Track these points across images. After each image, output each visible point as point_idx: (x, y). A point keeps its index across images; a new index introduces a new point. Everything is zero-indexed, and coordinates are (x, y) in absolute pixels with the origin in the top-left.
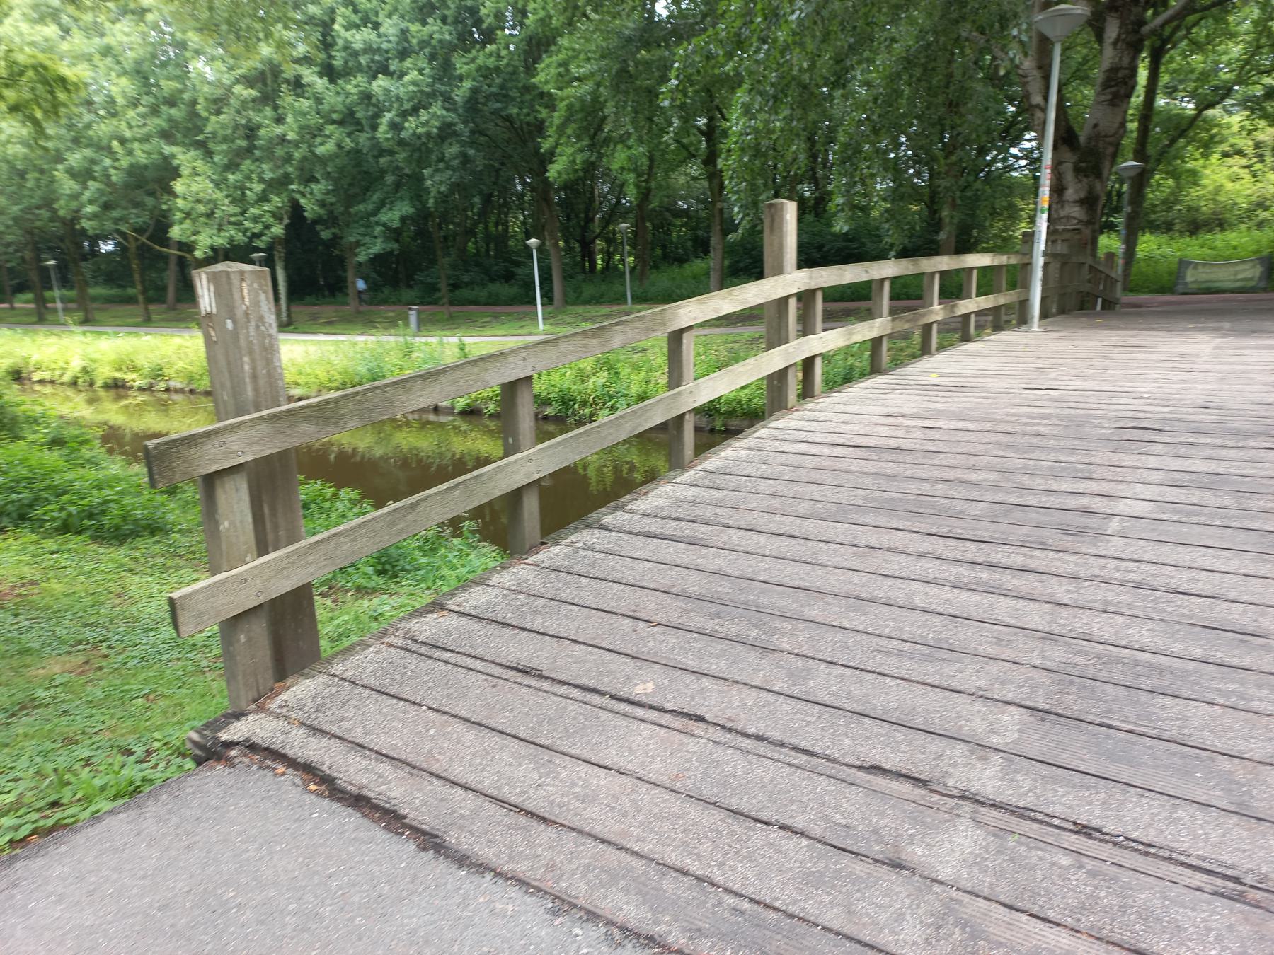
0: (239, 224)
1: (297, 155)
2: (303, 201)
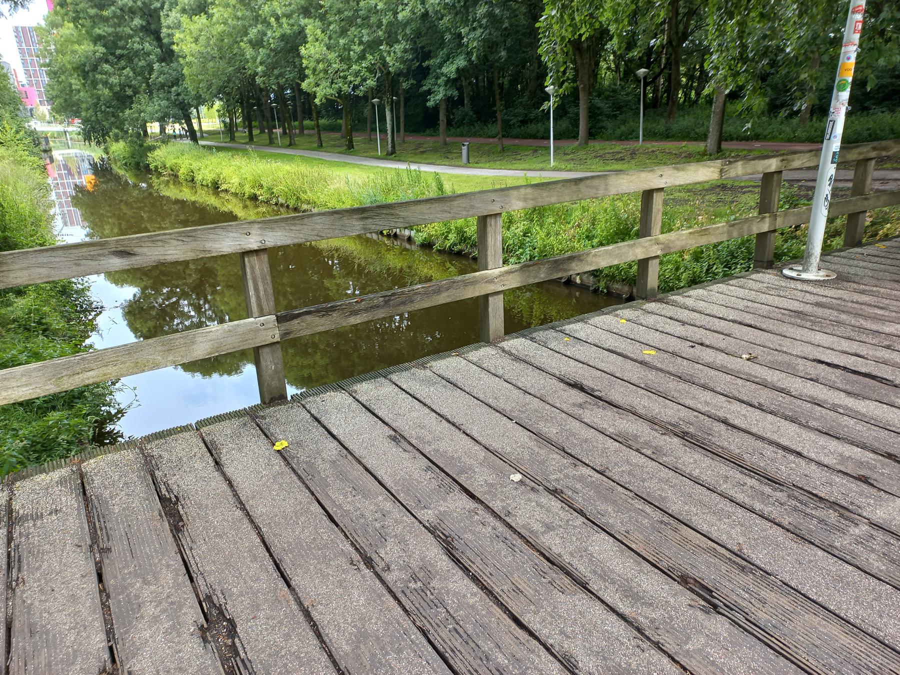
0: (345, 78)
2: (388, 59)
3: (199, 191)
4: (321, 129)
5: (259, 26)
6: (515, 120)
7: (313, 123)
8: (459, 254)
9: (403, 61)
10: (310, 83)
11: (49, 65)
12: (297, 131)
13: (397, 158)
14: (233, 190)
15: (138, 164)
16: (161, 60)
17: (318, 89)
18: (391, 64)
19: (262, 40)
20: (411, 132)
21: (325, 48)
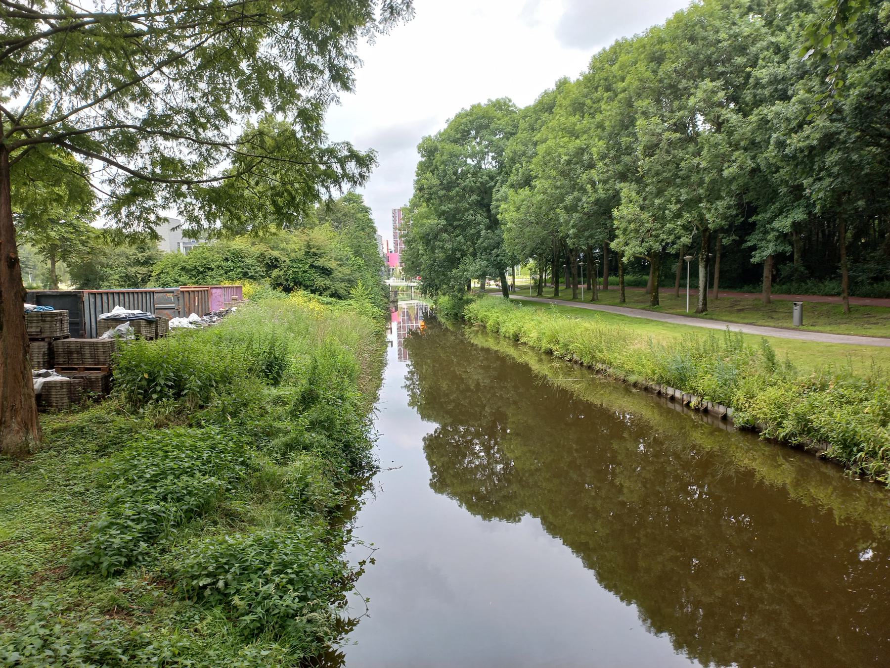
0: (657, 236)
1: (707, 179)
2: (708, 216)
3: (502, 342)
4: (625, 284)
5: (576, 193)
6: (864, 277)
7: (618, 279)
8: (799, 448)
9: (725, 217)
10: (620, 242)
11: (405, 236)
12: (601, 287)
13: (708, 316)
14: (531, 344)
15: (456, 314)
16: (488, 228)
17: (627, 248)
18: (711, 221)
19: (577, 205)
20: (724, 288)
21: (638, 209)
